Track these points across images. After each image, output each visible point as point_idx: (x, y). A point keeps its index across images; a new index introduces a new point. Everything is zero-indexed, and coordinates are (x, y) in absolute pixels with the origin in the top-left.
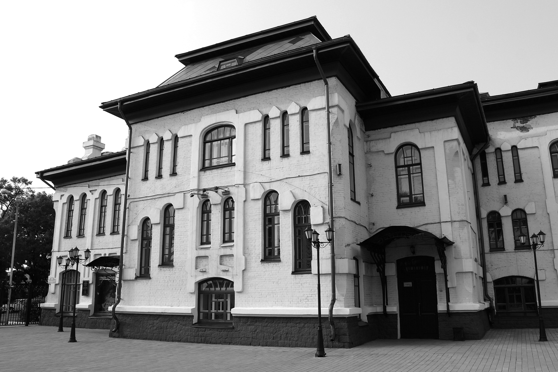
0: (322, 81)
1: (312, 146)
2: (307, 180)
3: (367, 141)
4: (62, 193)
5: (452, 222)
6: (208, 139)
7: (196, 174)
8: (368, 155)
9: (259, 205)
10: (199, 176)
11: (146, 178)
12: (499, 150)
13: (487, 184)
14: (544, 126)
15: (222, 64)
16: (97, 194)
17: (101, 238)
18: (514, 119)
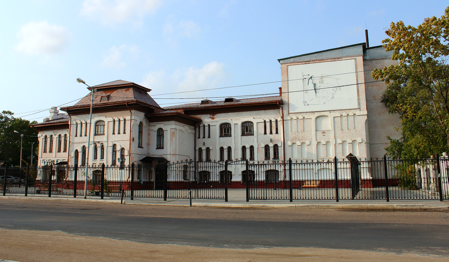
0: (129, 111)
1: (126, 131)
2: (124, 142)
3: (149, 126)
4: (42, 134)
5: (170, 154)
6: (97, 124)
7: (93, 137)
8: (149, 131)
9: (111, 148)
10: (94, 137)
11: (76, 136)
12: (204, 126)
13: (199, 138)
14: (219, 118)
15: (102, 97)
16: (57, 136)
17: (59, 153)
18: (210, 114)
